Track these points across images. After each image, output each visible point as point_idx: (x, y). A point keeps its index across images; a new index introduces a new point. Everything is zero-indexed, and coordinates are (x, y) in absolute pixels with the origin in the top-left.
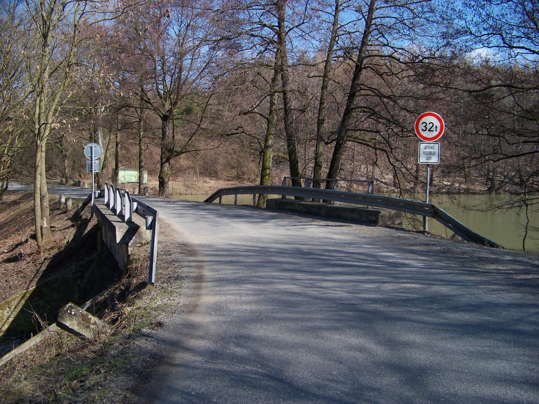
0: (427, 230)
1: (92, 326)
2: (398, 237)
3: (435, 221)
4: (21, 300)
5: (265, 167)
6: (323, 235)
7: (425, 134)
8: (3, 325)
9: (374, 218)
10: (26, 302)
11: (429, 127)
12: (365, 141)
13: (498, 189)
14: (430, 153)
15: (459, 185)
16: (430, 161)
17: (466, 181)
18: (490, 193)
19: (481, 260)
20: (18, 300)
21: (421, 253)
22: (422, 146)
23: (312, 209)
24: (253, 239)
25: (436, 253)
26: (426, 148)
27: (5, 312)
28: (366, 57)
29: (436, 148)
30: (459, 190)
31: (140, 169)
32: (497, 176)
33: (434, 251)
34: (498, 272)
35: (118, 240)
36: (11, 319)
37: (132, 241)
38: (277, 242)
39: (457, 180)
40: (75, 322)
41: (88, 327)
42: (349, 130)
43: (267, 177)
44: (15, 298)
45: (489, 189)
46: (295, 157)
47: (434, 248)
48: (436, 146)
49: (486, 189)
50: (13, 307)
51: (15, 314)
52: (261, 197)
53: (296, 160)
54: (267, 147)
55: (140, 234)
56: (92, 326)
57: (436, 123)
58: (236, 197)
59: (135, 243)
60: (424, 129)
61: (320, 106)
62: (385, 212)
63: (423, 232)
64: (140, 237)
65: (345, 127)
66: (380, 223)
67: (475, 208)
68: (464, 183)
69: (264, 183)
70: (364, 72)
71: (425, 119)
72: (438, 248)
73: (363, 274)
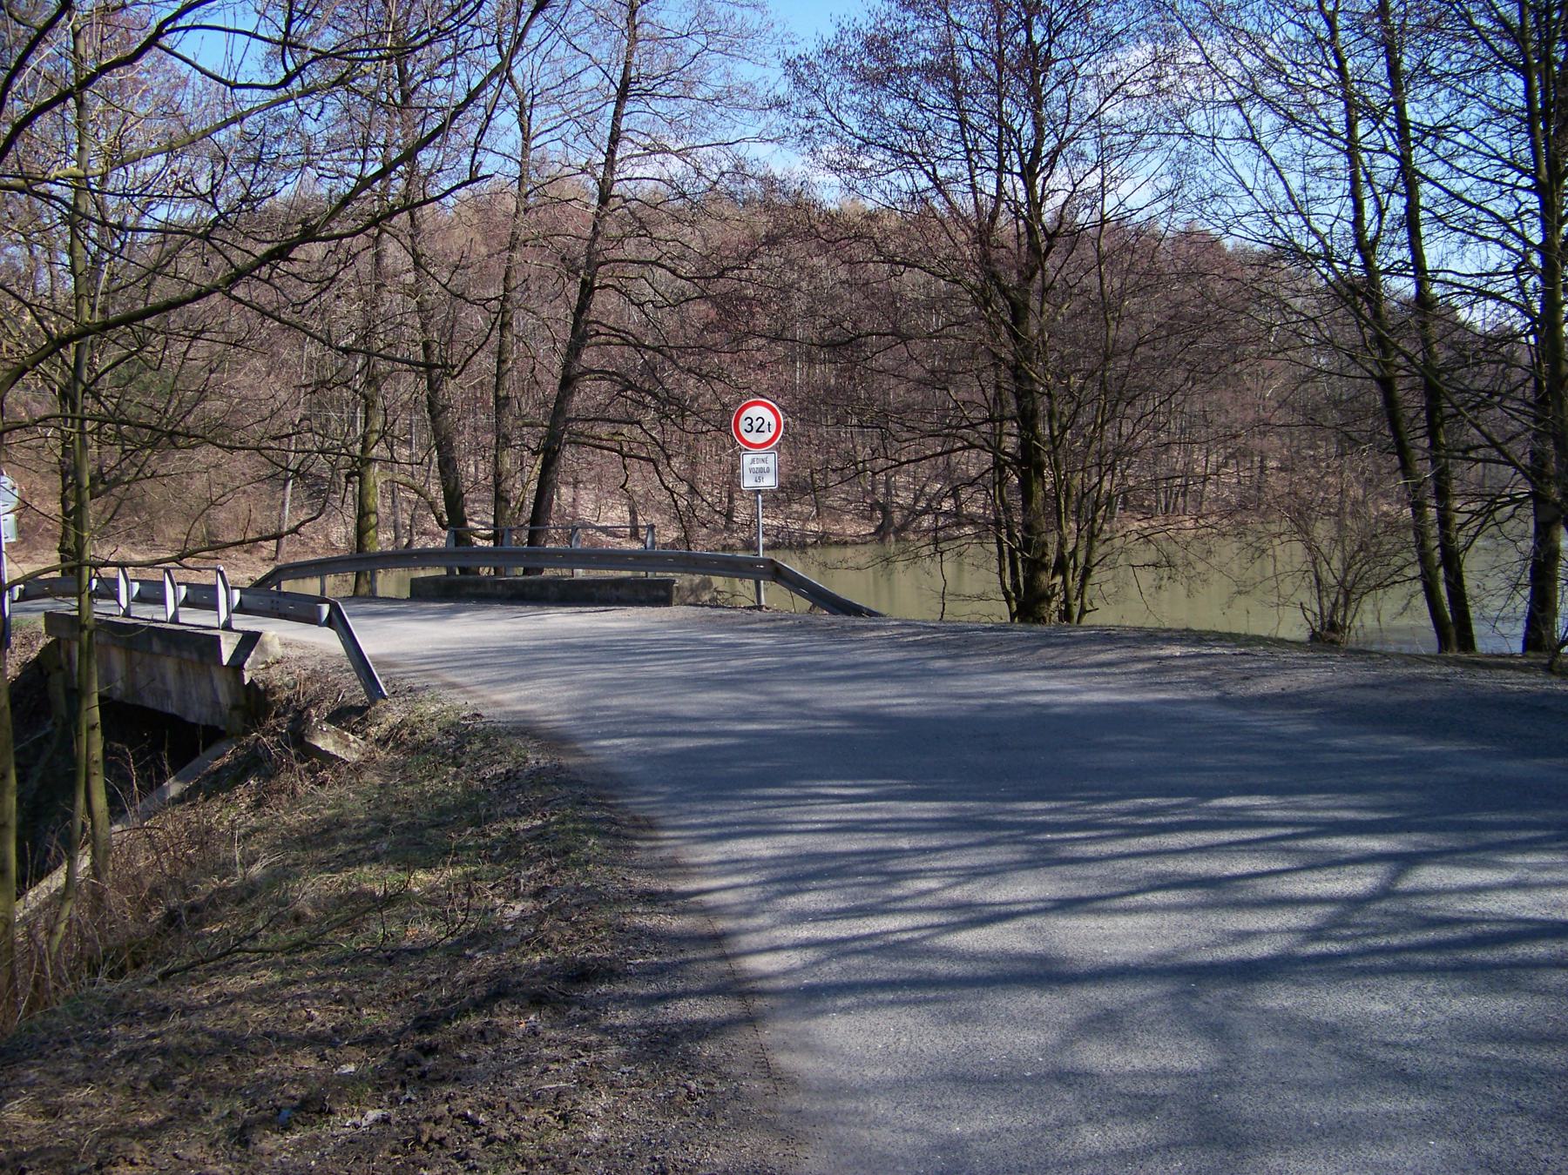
0: (763, 603)
1: (353, 745)
2: (721, 616)
3: (776, 588)
5: (367, 510)
6: (586, 625)
7: (749, 438)
9: (662, 593)
11: (756, 424)
12: (601, 439)
13: (904, 527)
14: (761, 470)
16: (761, 484)
17: (818, 514)
18: (882, 540)
19: (855, 629)
21: (767, 630)
22: (747, 459)
23: (527, 589)
25: (790, 629)
26: (753, 460)
28: (602, 264)
29: (771, 461)
30: (804, 536)
32: (898, 496)
33: (785, 626)
34: (880, 638)
35: (225, 660)
37: (249, 660)
38: (515, 639)
39: (796, 512)
40: (330, 741)
41: (348, 746)
42: (571, 420)
43: (372, 532)
45: (879, 529)
46: (456, 484)
47: (784, 623)
48: (771, 458)
49: (872, 530)
52: (362, 580)
53: (457, 493)
54: (367, 462)
55: (262, 645)
56: (353, 745)
57: (769, 417)
58: (322, 583)
59: (255, 662)
60: (749, 428)
61: (498, 368)
62: (682, 580)
63: (759, 608)
64: (264, 651)
65: (564, 414)
66: (676, 600)
67: (845, 565)
68: (814, 519)
69: (365, 546)
70: (598, 297)
71: (748, 412)
72: (790, 622)
73: (693, 657)
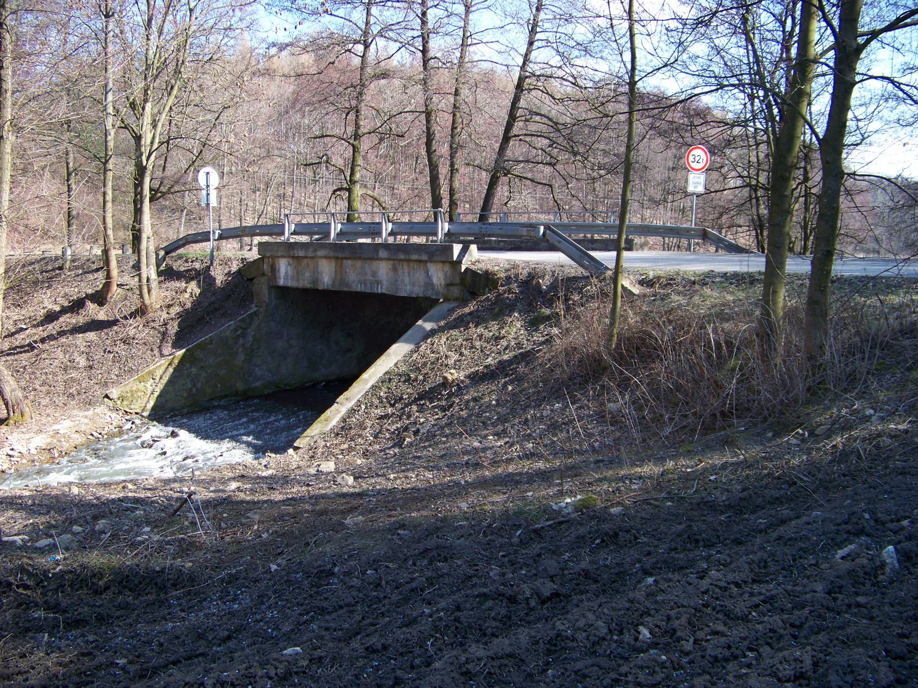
4: (167, 368)
7: (693, 165)
8: (148, 401)
10: (175, 369)
11: (697, 159)
14: (697, 183)
15: (748, 84)
20: (163, 368)
24: (279, 270)
27: (148, 385)
31: (877, 294)
36: (156, 394)
44: (160, 366)
50: (158, 377)
51: (161, 387)
57: (703, 156)
71: (694, 152)
